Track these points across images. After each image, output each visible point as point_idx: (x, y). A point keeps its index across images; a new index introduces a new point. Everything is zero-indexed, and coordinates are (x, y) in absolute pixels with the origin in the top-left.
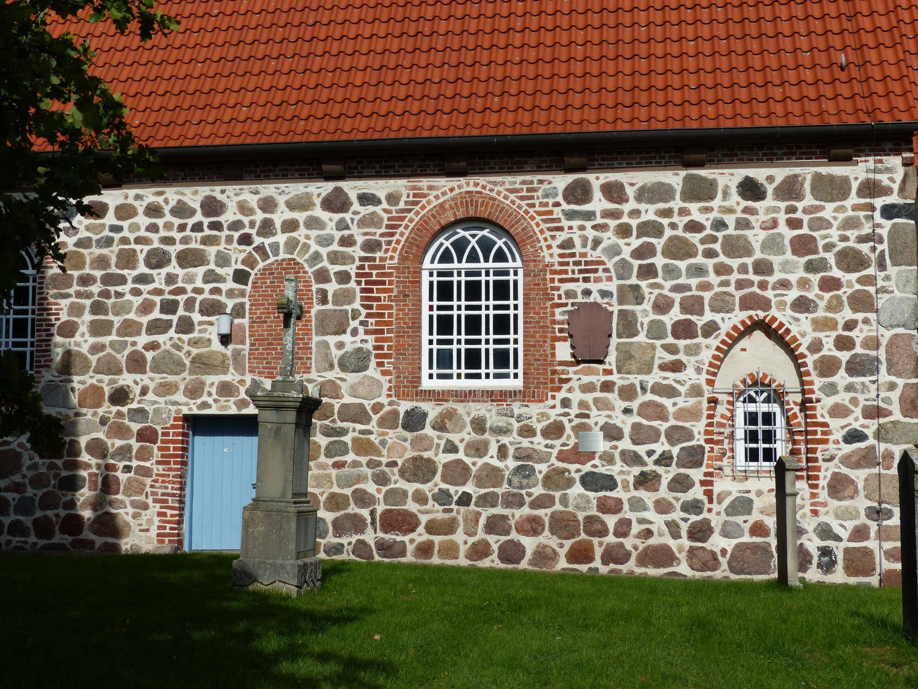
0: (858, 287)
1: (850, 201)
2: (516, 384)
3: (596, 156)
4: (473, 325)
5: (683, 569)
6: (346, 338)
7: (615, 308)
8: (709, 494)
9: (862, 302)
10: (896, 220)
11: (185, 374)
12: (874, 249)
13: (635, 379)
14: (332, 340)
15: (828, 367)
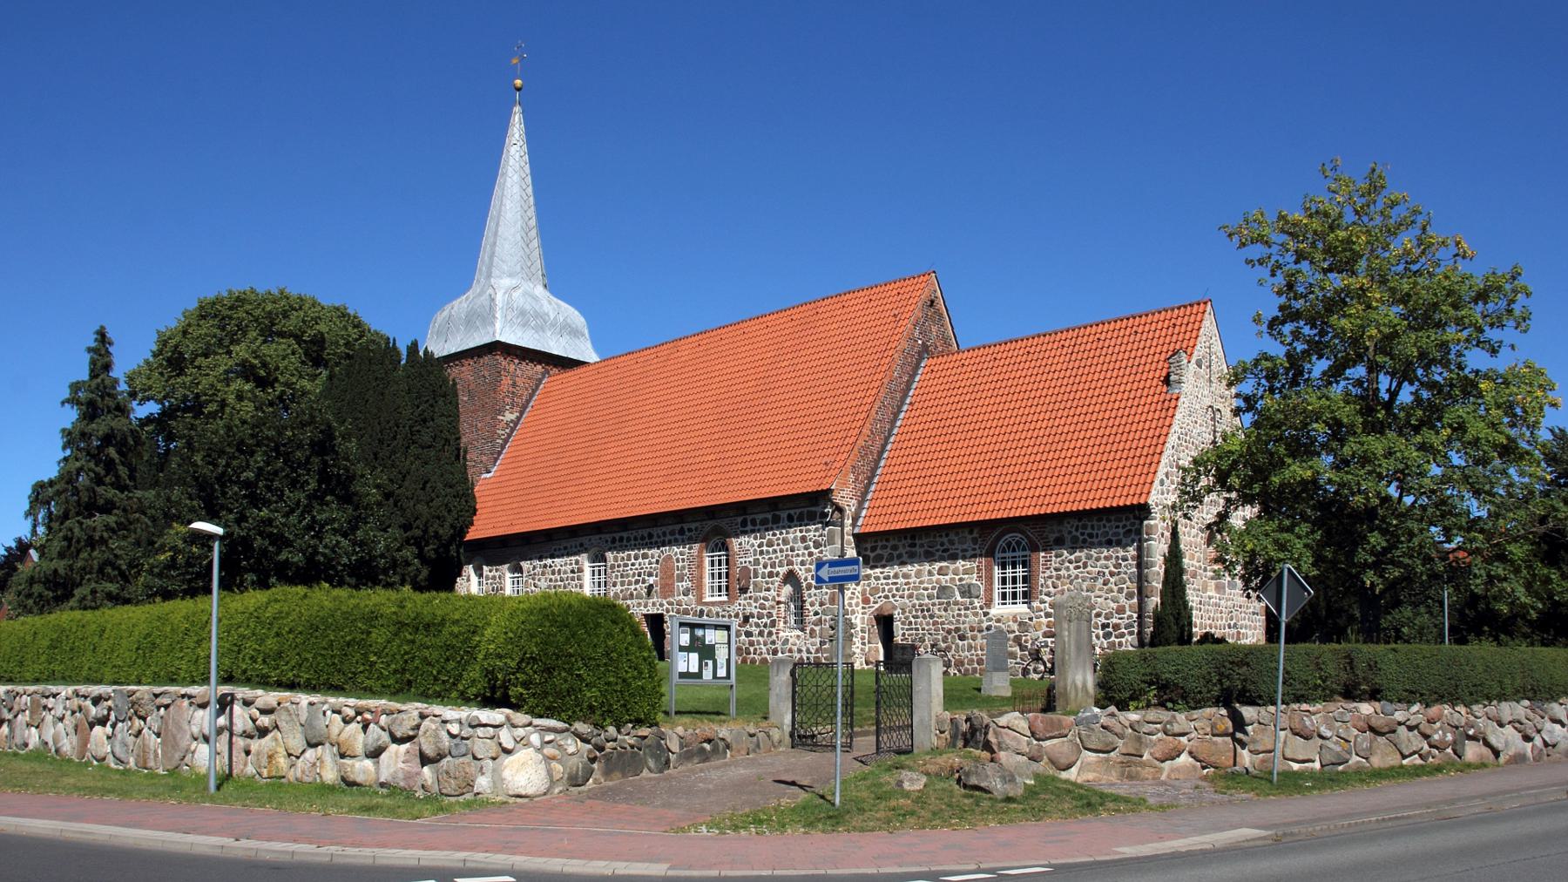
2: (725, 598)
4: (1014, 580)
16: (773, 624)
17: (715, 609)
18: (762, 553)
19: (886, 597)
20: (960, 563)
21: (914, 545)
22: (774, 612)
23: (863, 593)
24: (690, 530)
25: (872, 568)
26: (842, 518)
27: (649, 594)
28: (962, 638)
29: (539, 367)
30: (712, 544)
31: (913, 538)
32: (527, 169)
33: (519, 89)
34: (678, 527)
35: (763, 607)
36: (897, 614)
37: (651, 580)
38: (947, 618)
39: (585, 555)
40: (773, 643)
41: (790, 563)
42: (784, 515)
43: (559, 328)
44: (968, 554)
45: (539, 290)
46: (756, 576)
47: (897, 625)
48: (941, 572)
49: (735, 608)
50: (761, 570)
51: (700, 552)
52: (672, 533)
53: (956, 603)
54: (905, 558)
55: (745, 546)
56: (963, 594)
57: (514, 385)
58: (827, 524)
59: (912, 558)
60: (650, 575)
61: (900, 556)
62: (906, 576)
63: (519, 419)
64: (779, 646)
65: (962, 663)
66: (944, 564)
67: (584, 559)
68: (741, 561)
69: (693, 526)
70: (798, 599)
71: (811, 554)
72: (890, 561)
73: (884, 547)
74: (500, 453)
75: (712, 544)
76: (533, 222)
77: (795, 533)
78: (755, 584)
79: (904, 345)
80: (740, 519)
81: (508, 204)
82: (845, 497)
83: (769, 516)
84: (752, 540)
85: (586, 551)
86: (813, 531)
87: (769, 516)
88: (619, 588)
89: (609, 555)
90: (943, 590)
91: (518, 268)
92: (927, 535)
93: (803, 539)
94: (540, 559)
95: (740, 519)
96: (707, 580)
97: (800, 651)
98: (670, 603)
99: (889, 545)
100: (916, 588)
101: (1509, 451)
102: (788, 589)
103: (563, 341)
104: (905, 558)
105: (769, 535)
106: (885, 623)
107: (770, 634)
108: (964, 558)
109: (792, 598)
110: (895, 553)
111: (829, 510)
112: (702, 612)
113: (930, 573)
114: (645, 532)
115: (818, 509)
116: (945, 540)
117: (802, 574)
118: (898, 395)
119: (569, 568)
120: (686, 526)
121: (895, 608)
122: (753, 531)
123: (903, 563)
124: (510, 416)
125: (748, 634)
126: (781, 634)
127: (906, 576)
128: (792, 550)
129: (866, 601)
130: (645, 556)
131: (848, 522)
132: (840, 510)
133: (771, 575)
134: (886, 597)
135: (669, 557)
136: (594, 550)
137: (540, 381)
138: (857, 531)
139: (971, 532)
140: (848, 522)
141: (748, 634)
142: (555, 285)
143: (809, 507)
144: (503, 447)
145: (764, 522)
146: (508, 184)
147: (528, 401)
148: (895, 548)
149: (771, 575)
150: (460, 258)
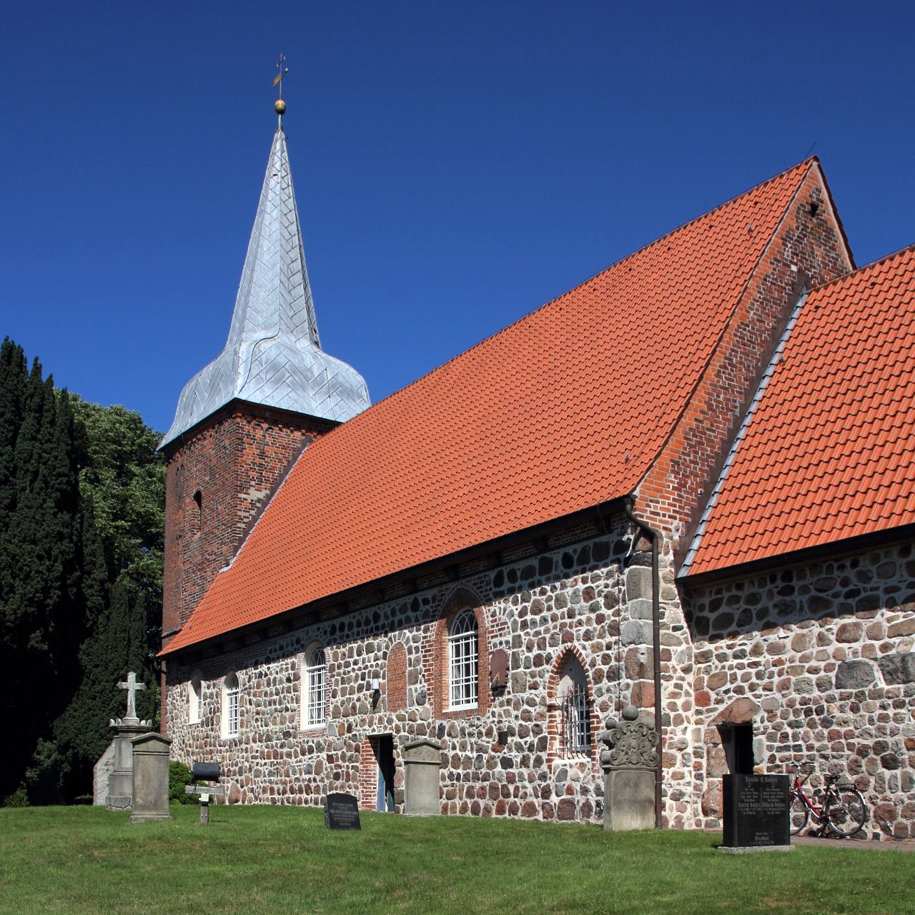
0: (613, 618)
1: (888, 631)
2: (474, 705)
3: (813, 622)
5: (540, 817)
6: (418, 686)
7: (510, 652)
8: (550, 767)
9: (614, 629)
10: (632, 567)
11: (537, 707)
12: (620, 591)
13: (520, 695)
14: (413, 687)
15: (598, 679)
16: (543, 745)
17: (459, 724)
18: (524, 625)
19: (739, 690)
20: (883, 616)
21: (788, 591)
22: (544, 724)
23: (698, 685)
24: (426, 601)
25: (713, 639)
26: (655, 550)
27: (374, 704)
28: (890, 763)
29: (298, 434)
30: (456, 621)
31: (787, 576)
32: (291, 203)
33: (281, 112)
34: (409, 599)
35: (527, 717)
36: (758, 721)
37: (375, 684)
38: (859, 725)
39: (301, 655)
40: (543, 777)
41: (568, 638)
42: (557, 557)
43: (330, 387)
44: (899, 596)
45: (305, 345)
46: (516, 666)
47: (760, 741)
48: (844, 635)
49: (487, 720)
50: (524, 654)
51: (439, 634)
52: (403, 610)
53: (877, 694)
54: (773, 616)
55: (500, 614)
56: (890, 676)
57: (262, 455)
58: (627, 562)
59: (787, 614)
60: (376, 676)
61: (763, 614)
62: (774, 649)
63: (269, 497)
64: (551, 782)
65: (892, 815)
66: (850, 620)
67: (300, 660)
68: (498, 641)
69: (429, 594)
70: (582, 698)
71: (600, 619)
72: (744, 624)
73: (734, 600)
74: (241, 541)
75: (456, 621)
76: (297, 266)
77: (574, 586)
78: (515, 679)
79: (765, 268)
80: (492, 575)
81: (265, 244)
82: (660, 511)
83: (535, 562)
84: (511, 607)
85: (302, 648)
86: (603, 578)
87: (535, 562)
88: (339, 698)
89: (328, 651)
90: (849, 670)
91: (276, 317)
92: (814, 568)
93: (588, 594)
94: (255, 665)
95: (492, 575)
96: (450, 677)
97: (585, 791)
98: (401, 718)
99: (744, 594)
100: (794, 670)
101: (629, 900)
102: (566, 684)
103: (331, 402)
104: (773, 616)
105: (535, 595)
106: (737, 737)
107: (538, 761)
108: (891, 605)
109: (571, 700)
110: (754, 609)
111: (630, 536)
112: (442, 728)
113: (822, 640)
114: (368, 613)
115: (611, 538)
116: (850, 573)
117: (586, 653)
118: (758, 350)
119: (284, 675)
120: (420, 597)
121: (755, 709)
122: (511, 591)
123: (769, 626)
124: (255, 495)
125: (507, 763)
126: (557, 762)
127: (774, 649)
128: (571, 615)
129: (702, 699)
130: (370, 649)
131: (667, 558)
132: (649, 534)
133: (538, 661)
134: (739, 690)
135: (400, 647)
136: (312, 647)
137: (299, 451)
138: (683, 573)
139: (905, 551)
140: (667, 558)
141: (507, 763)
142: (331, 338)
143: (594, 535)
144: (246, 533)
145: (528, 573)
146: (266, 222)
147: (282, 477)
148: (753, 599)
149: (538, 661)
150: (207, 318)
